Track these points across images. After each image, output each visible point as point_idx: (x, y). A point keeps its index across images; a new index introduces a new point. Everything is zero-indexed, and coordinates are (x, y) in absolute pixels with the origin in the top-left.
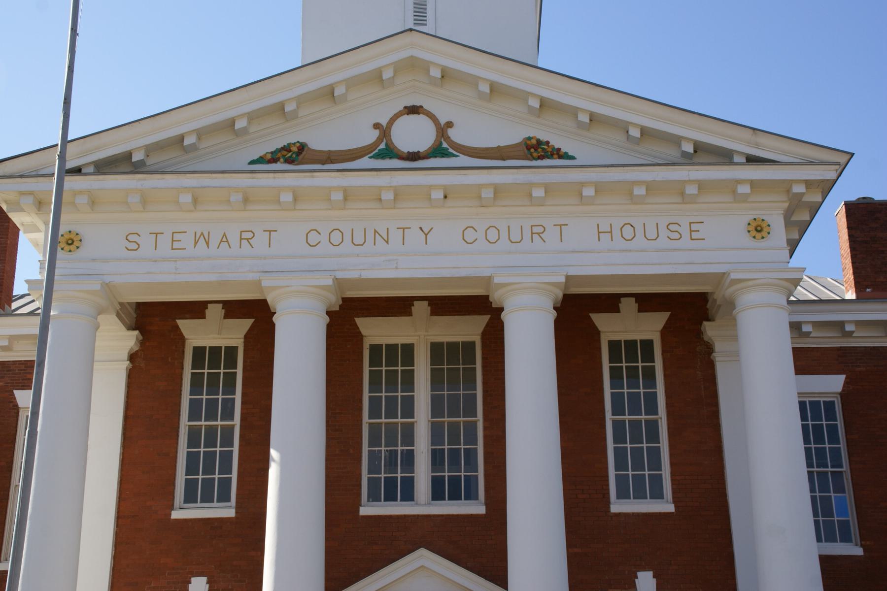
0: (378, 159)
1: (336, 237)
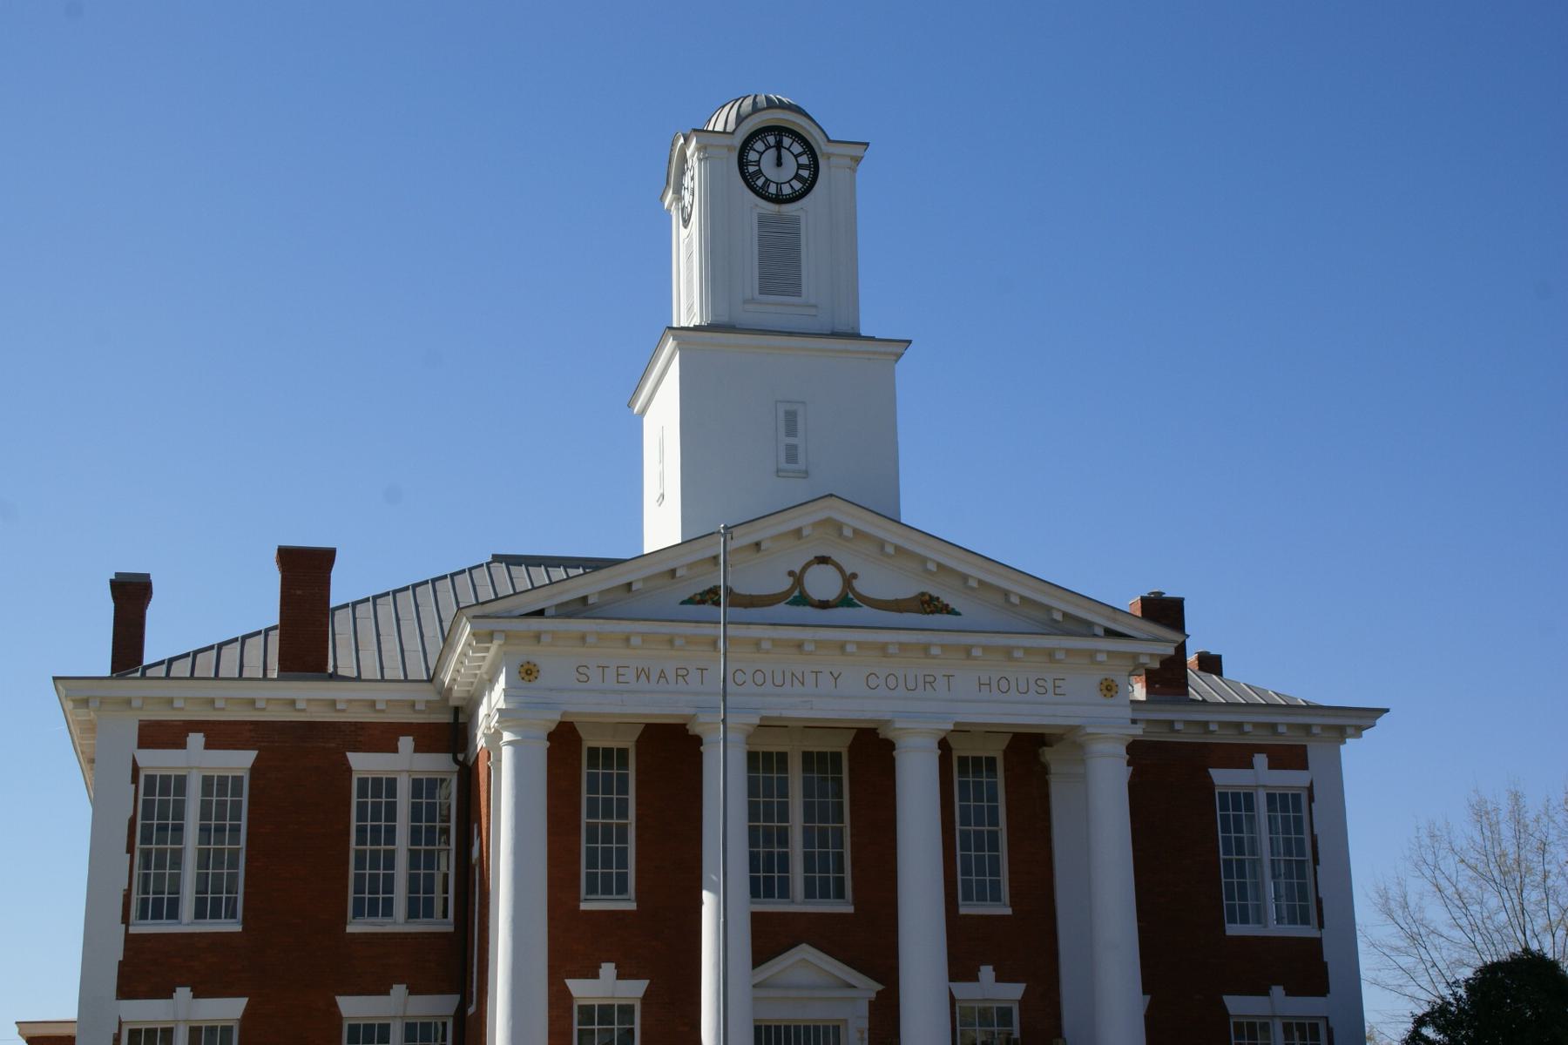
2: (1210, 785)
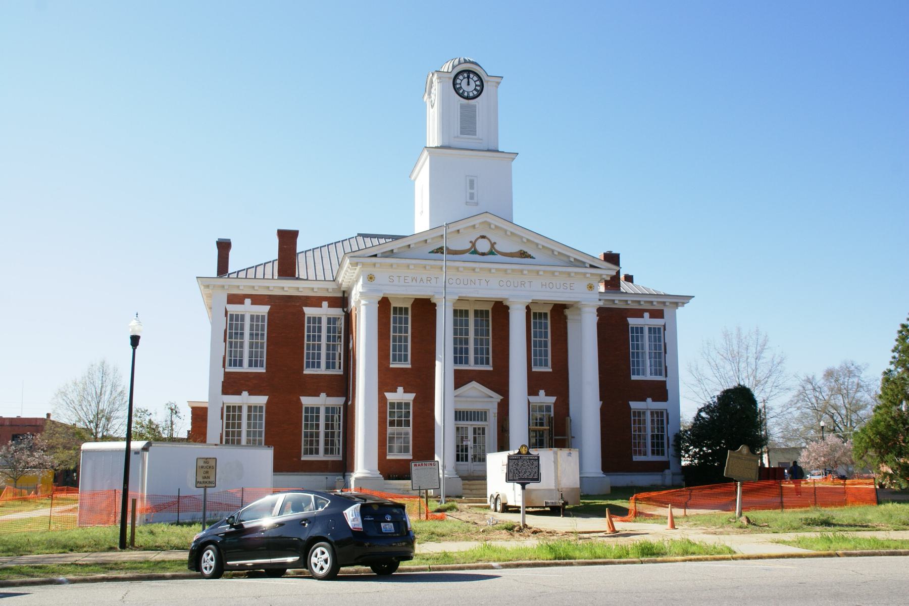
0: (473, 254)
1: (458, 282)
2: (628, 325)
